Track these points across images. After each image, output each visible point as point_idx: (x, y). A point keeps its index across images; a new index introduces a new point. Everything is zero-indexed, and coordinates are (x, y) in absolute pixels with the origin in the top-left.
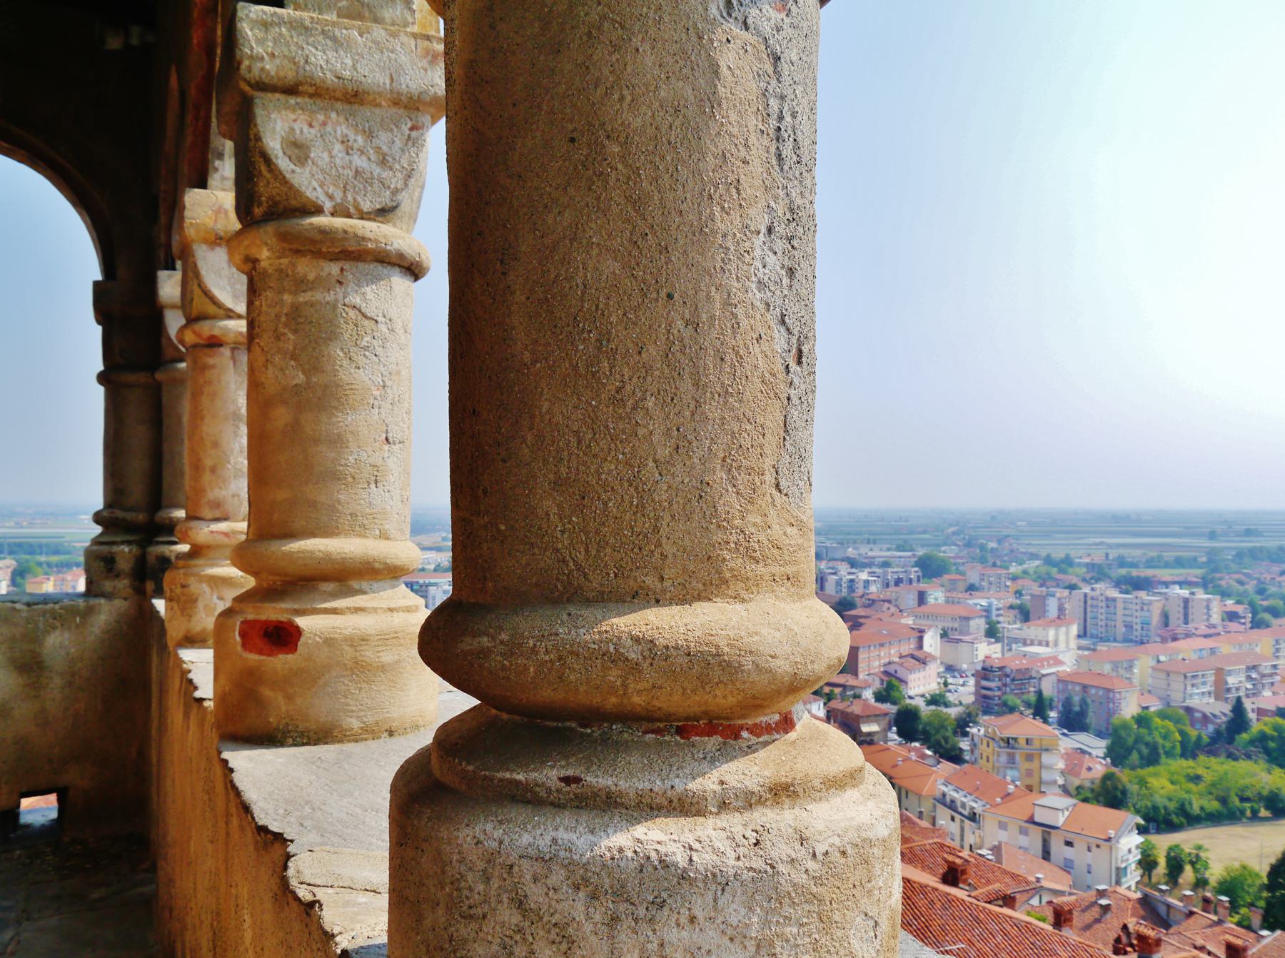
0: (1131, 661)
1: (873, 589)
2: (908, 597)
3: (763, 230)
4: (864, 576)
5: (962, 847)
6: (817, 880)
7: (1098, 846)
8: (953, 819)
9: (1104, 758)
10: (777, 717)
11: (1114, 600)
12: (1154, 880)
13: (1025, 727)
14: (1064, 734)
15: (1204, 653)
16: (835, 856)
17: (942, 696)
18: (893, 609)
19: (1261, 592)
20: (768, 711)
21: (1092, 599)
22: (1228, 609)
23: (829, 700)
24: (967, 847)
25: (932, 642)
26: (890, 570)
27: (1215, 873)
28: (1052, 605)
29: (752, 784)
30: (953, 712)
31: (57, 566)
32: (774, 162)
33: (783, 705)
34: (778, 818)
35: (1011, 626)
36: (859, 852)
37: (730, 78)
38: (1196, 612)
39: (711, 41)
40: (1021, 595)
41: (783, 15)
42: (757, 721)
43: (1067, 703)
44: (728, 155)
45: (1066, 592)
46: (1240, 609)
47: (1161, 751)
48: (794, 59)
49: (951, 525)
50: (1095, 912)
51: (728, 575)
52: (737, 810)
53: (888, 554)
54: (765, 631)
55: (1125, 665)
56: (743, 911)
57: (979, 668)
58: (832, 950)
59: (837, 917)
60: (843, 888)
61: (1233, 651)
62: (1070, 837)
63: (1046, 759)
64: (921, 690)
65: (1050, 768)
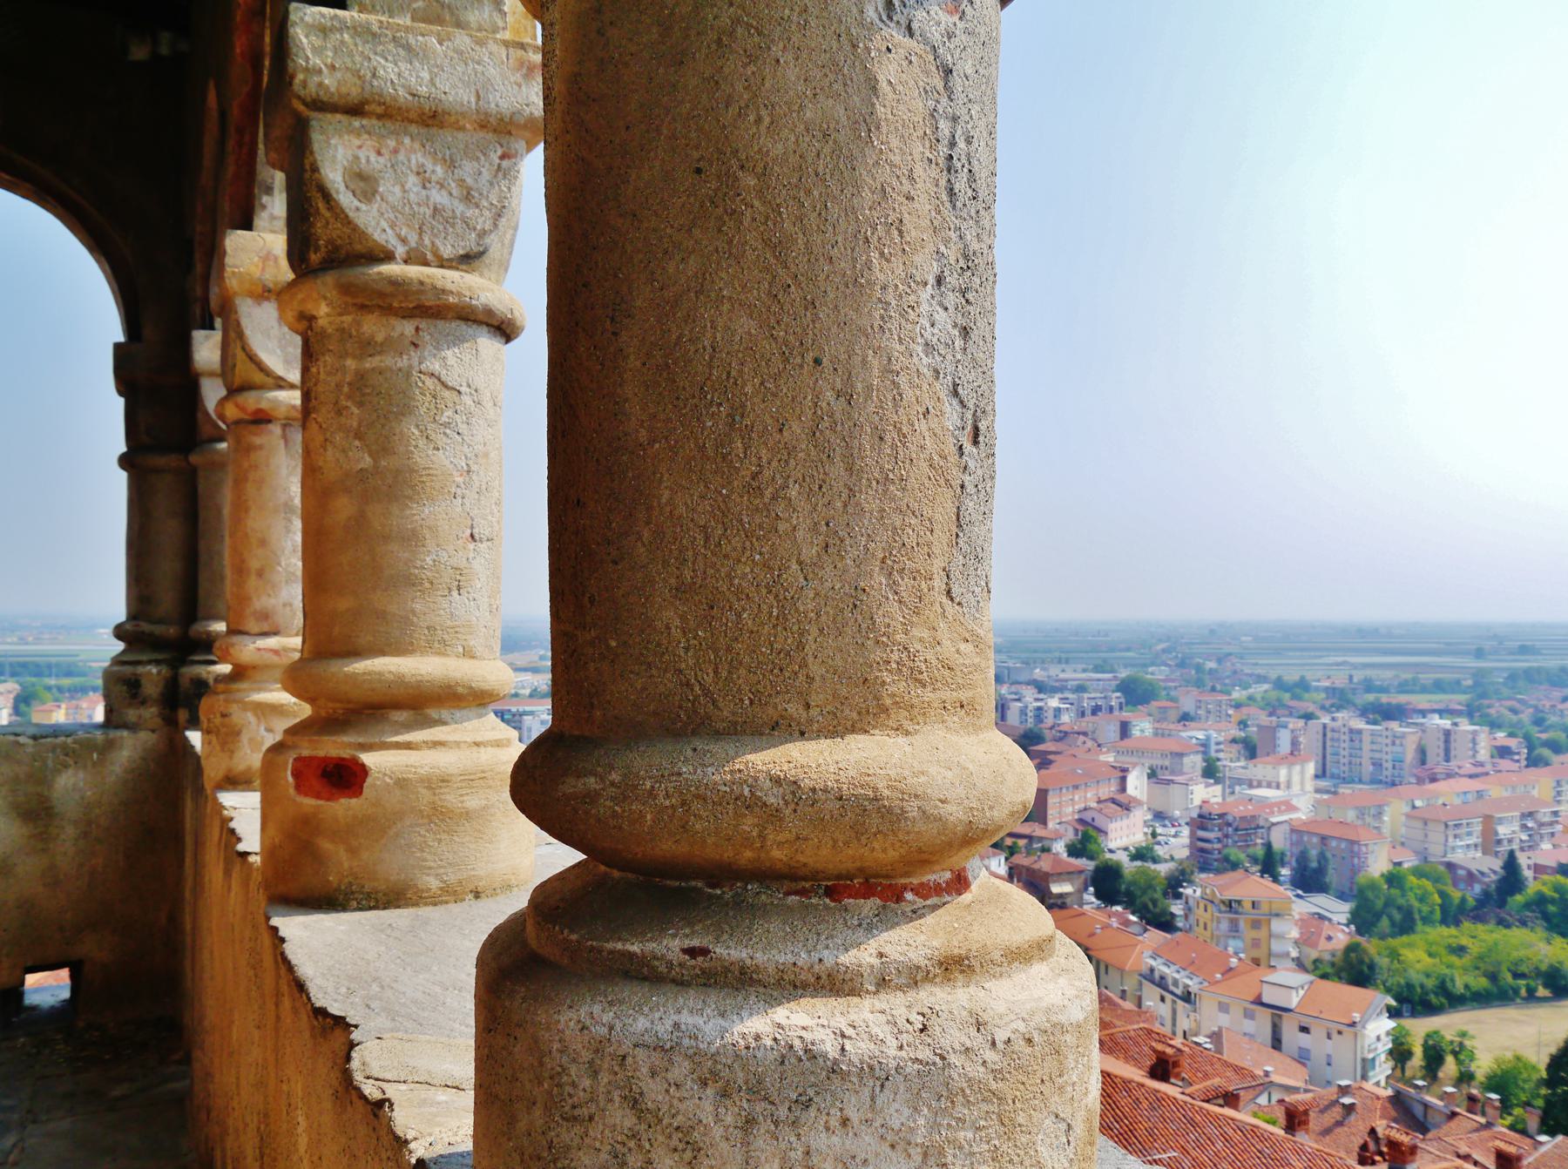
0: (1380, 806)
1: (1065, 718)
2: (1108, 729)
3: (931, 280)
4: (1054, 702)
5: (1174, 1033)
6: (997, 1074)
7: (1340, 1033)
8: (1163, 999)
9: (1347, 925)
10: (948, 875)
11: (1360, 732)
12: (1408, 1073)
13: (1251, 887)
14: (1298, 896)
15: (1470, 797)
16: (1019, 1045)
17: (1149, 849)
18: (1090, 744)
19: (1539, 722)
20: (937, 867)
21: (1333, 730)
22: (1498, 744)
23: (1012, 854)
24: (1180, 1034)
25: (1137, 783)
26: (1086, 695)
27: (1483, 1065)
28: (1284, 739)
29: (918, 956)
30: (1163, 869)
31: (69, 690)
32: (945, 197)
33: (956, 861)
34: (949, 998)
35: (1233, 764)
36: (1048, 1040)
37: (891, 95)
38: (1460, 747)
39: (868, 50)
40: (1246, 726)
41: (956, 18)
42: (924, 879)
43: (1303, 858)
44: (888, 189)
45: (1301, 723)
46: (1513, 743)
47: (1417, 916)
48: (969, 71)
49: (1160, 641)
50: (1336, 1113)
51: (888, 702)
52: (900, 988)
53: (1084, 675)
54: (933, 770)
55: (1373, 811)
56: (906, 1112)
57: (1195, 815)
58: (1016, 1159)
59: (1021, 1119)
60: (1028, 1083)
61: (1505, 794)
62: (1306, 1022)
63: (1277, 926)
64: (1124, 842)
65: (1281, 937)
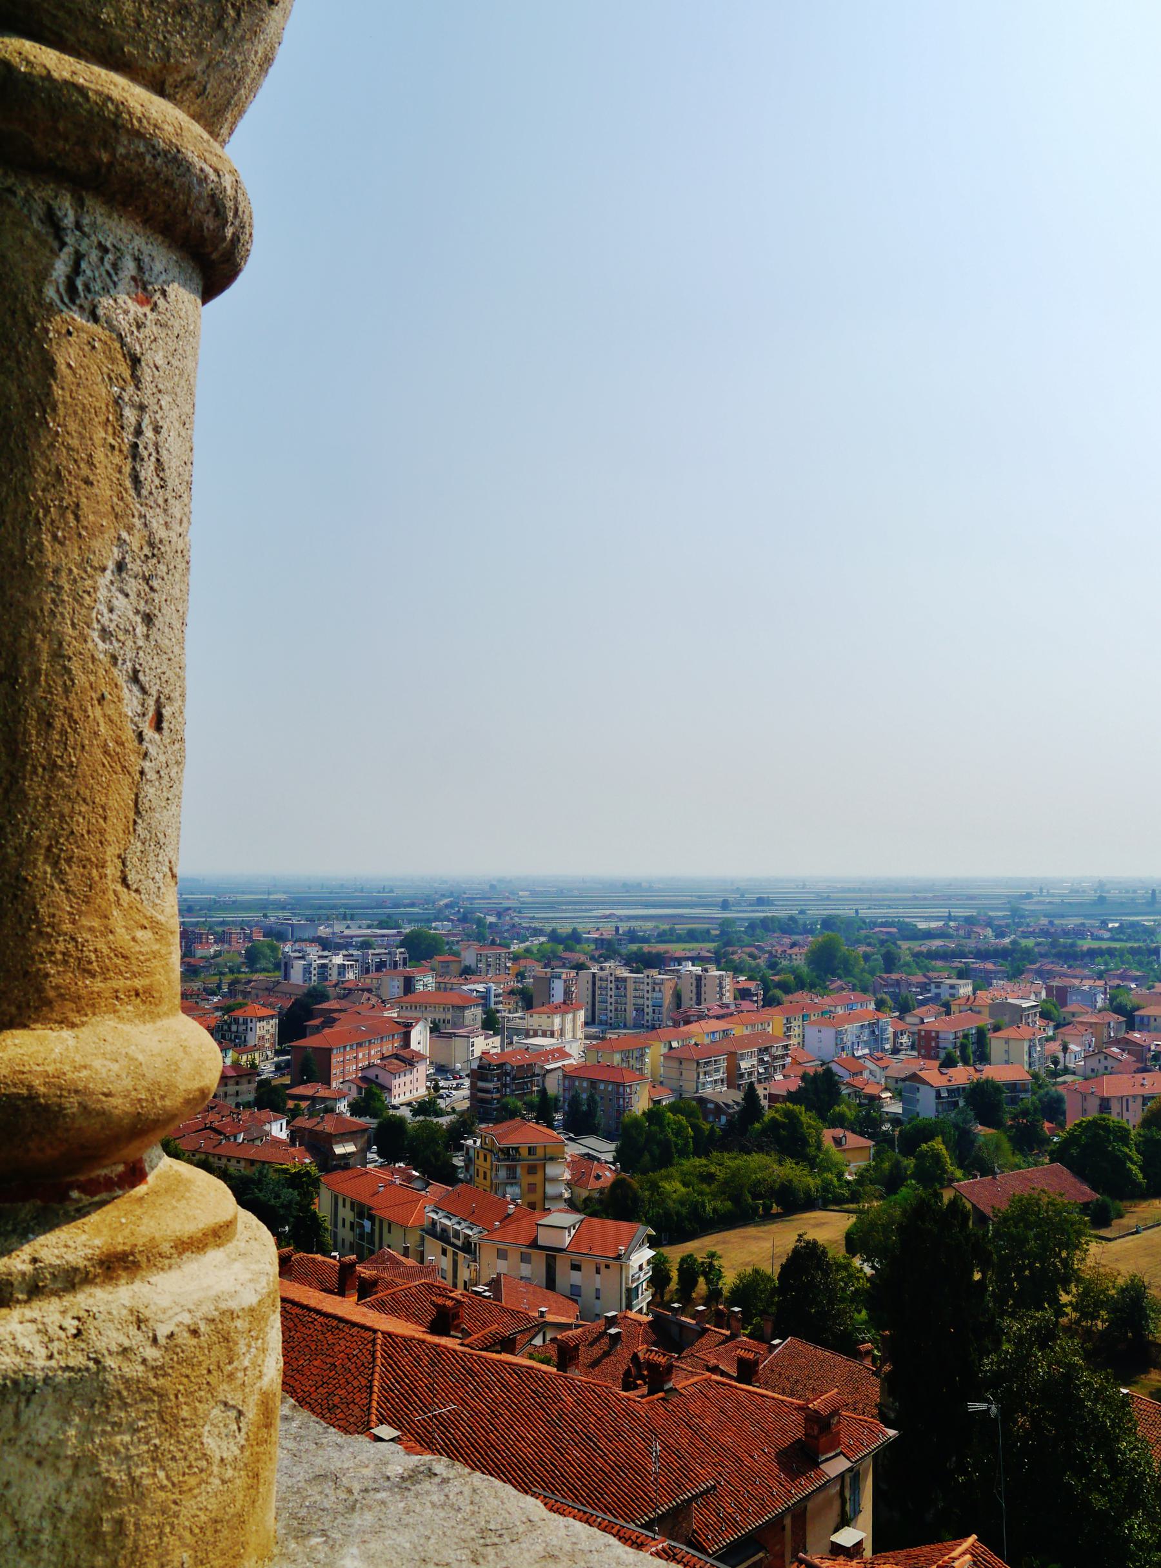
0: (642, 1049)
1: (350, 975)
2: (393, 986)
3: (111, 565)
4: (338, 960)
5: (455, 1285)
6: (158, 1371)
7: (607, 1267)
8: (444, 1252)
9: (613, 1163)
10: (121, 1168)
11: (625, 980)
12: (667, 1298)
13: (528, 1134)
14: (570, 1139)
15: (716, 1035)
16: (184, 1338)
17: (432, 1103)
18: (374, 1000)
19: (772, 966)
20: (106, 1162)
21: (601, 979)
22: (740, 986)
23: (294, 1117)
24: (460, 1284)
25: (421, 1038)
26: (371, 952)
27: (729, 1281)
28: (558, 987)
29: (76, 1258)
30: (444, 1121)
32: (128, 484)
33: (129, 1152)
34: (110, 1297)
35: (511, 1016)
36: (221, 1331)
37: (70, 378)
38: (709, 991)
39: (47, 331)
40: (523, 977)
41: (147, 309)
42: (93, 1175)
43: (574, 1101)
44: (64, 473)
45: (573, 973)
46: (752, 986)
47: (674, 1150)
48: (159, 362)
49: (443, 896)
50: (604, 1343)
51: (52, 994)
52: (55, 1293)
53: (369, 931)
54: (97, 1063)
55: (636, 1054)
56: (55, 1424)
57: (475, 1066)
58: (179, 1455)
59: (185, 1413)
60: (192, 1375)
61: (746, 1032)
62: (577, 1258)
63: (552, 1170)
64: (408, 1097)
65: (554, 1180)
